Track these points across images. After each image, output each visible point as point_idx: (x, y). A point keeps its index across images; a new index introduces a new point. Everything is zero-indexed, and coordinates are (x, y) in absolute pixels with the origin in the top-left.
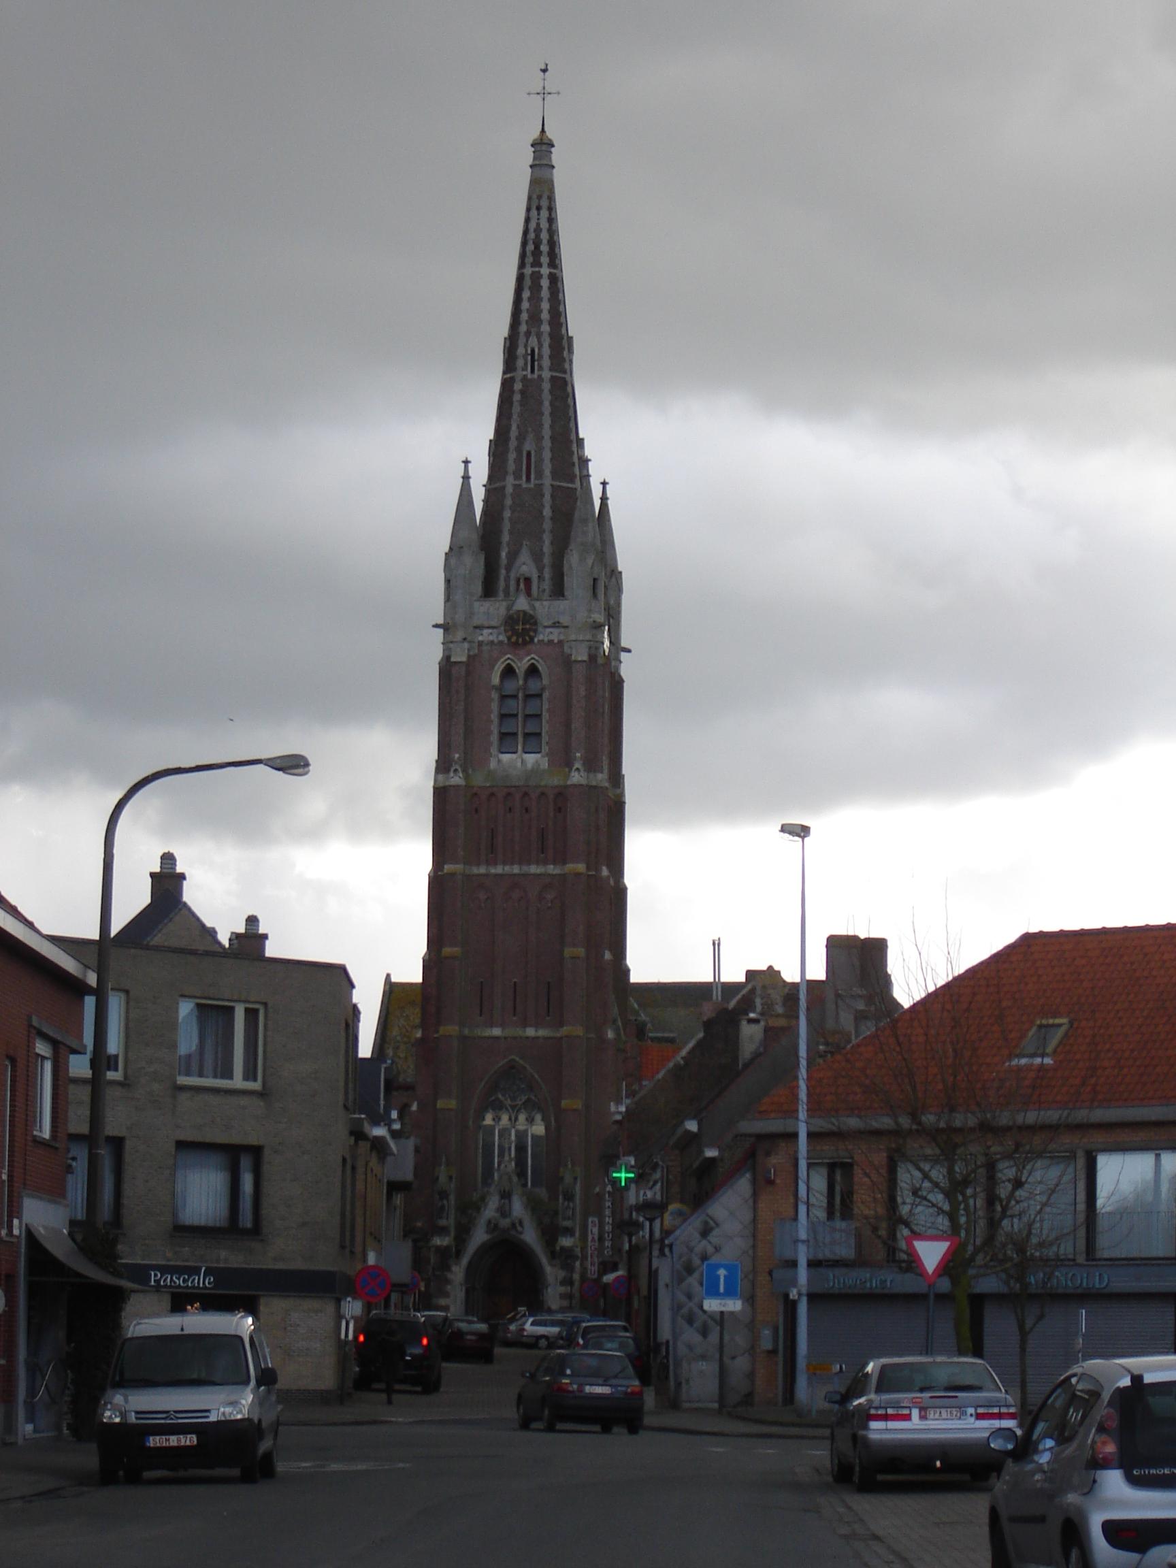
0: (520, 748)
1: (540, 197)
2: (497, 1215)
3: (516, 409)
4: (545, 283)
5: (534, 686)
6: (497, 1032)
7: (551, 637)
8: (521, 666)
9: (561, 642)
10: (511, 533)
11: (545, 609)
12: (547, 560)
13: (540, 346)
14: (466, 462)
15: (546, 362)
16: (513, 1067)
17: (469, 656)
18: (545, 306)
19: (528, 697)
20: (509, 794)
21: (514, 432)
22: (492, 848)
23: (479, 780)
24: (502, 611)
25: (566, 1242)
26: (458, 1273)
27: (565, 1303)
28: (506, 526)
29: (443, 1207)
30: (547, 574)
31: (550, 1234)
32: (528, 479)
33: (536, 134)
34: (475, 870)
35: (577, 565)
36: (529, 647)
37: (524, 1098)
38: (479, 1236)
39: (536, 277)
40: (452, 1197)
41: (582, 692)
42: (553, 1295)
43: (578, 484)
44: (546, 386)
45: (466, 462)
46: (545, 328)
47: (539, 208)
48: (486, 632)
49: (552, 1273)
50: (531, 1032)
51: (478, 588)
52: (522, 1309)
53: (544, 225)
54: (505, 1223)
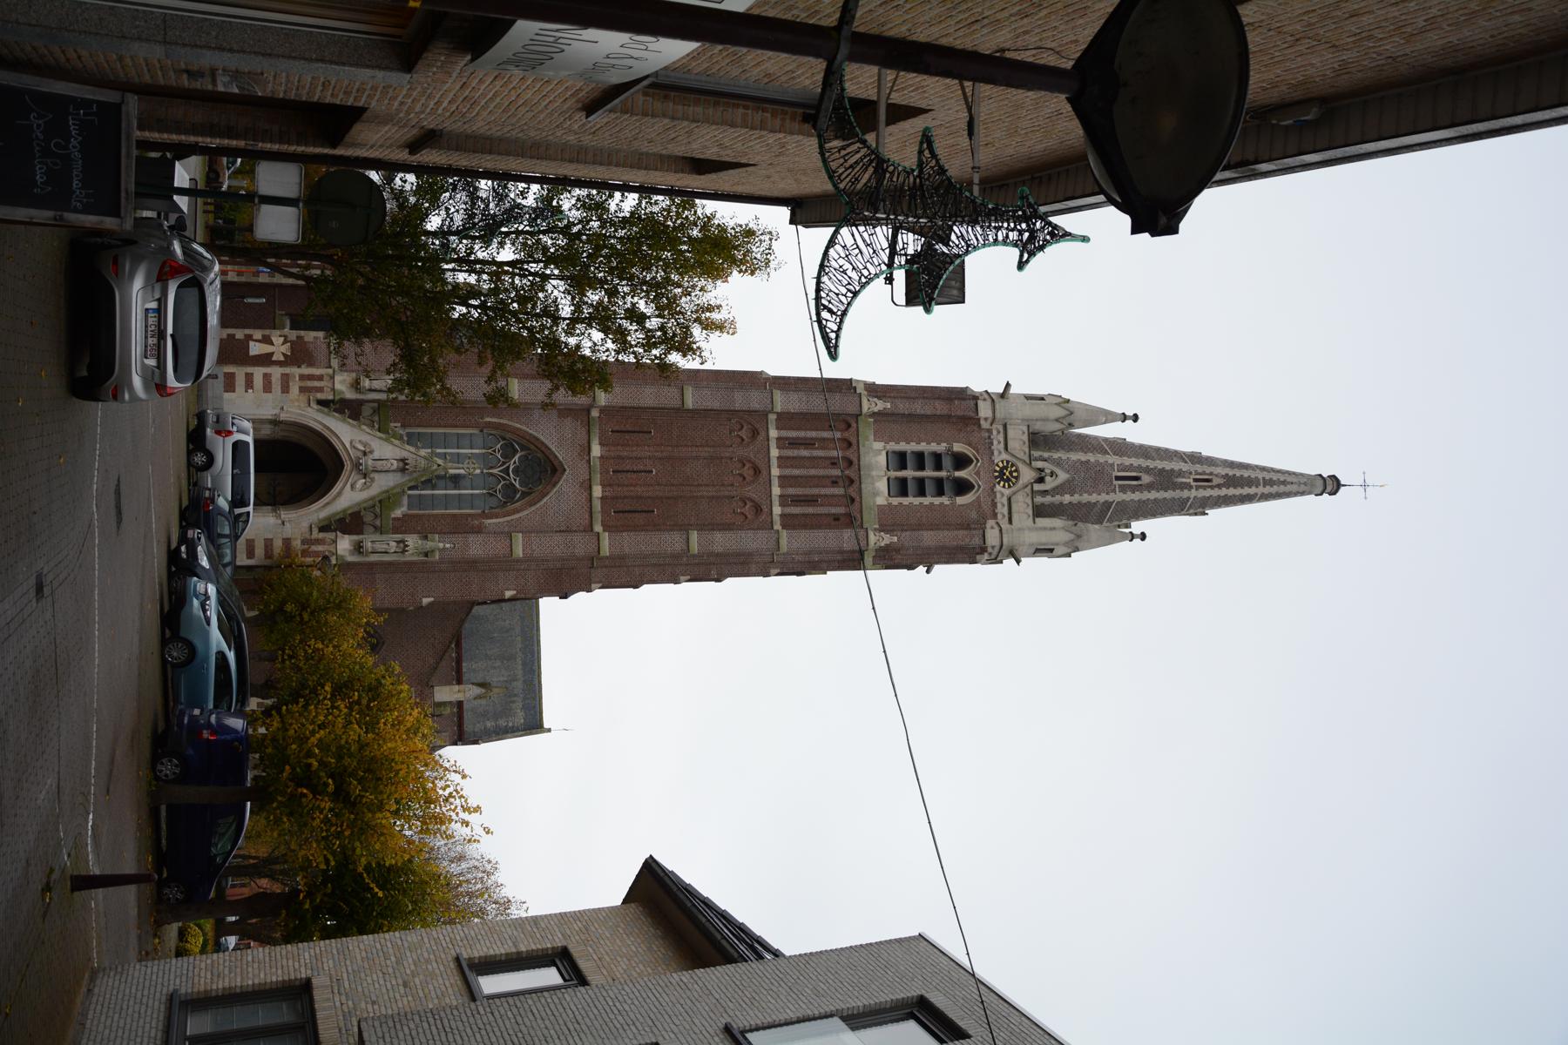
16: (554, 470)
28: (1082, 457)
30: (1048, 499)
32: (1118, 478)
45: (1135, 418)
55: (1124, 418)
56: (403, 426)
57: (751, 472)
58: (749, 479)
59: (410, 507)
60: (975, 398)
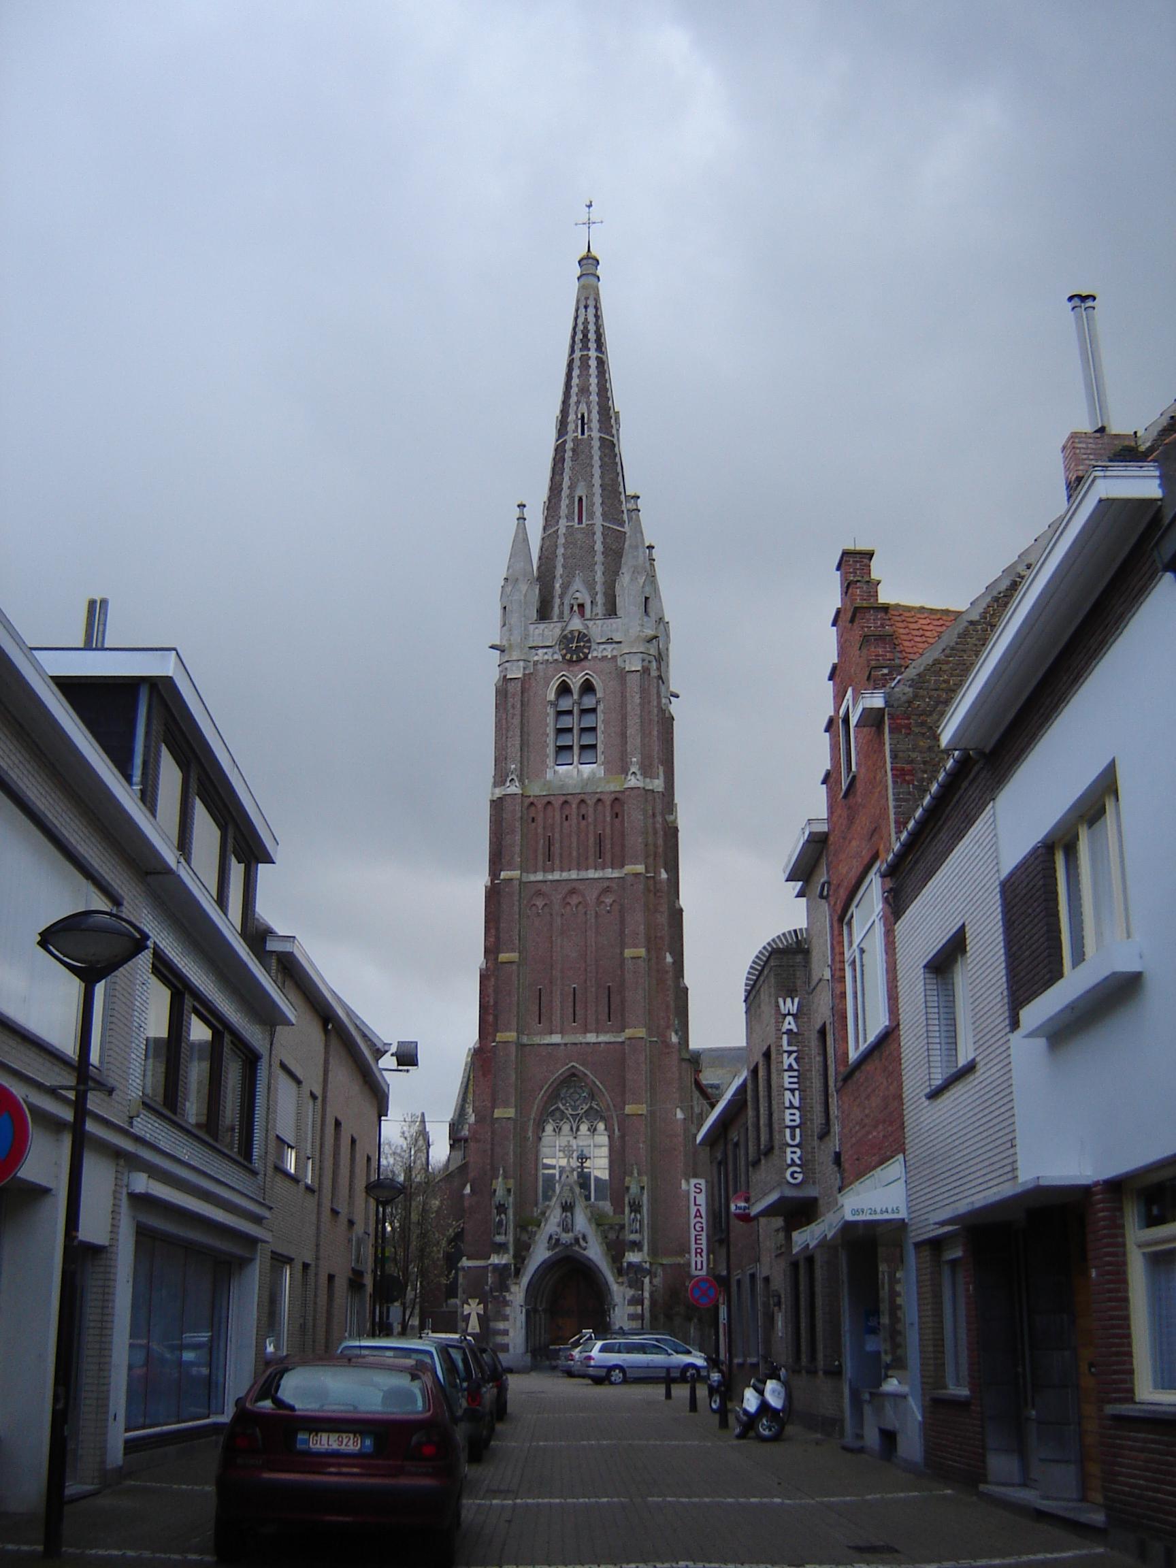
0: (576, 758)
1: (587, 299)
2: (559, 1230)
3: (568, 464)
4: (593, 363)
5: (588, 702)
6: (556, 1039)
7: (605, 653)
8: (575, 683)
9: (614, 657)
10: (563, 566)
11: (598, 629)
12: (599, 588)
13: (590, 412)
14: (522, 506)
15: (595, 425)
16: (574, 1075)
17: (524, 675)
18: (594, 381)
19: (584, 712)
20: (566, 802)
21: (566, 483)
22: (549, 857)
23: (535, 790)
24: (558, 631)
25: (633, 1257)
26: (517, 1294)
27: (635, 1325)
28: (560, 561)
29: (501, 1221)
30: (600, 599)
31: (616, 1249)
32: (580, 521)
33: (584, 252)
34: (532, 878)
35: (628, 589)
36: (583, 663)
37: (586, 1107)
38: (540, 1254)
39: (585, 360)
40: (511, 1212)
41: (637, 700)
42: (621, 1315)
43: (627, 529)
44: (596, 444)
46: (594, 398)
47: (586, 307)
48: (541, 651)
49: (619, 1291)
50: (591, 1038)
51: (534, 615)
52: (587, 1332)
53: (591, 319)
54: (566, 1238)
55: (522, 519)
56: (536, 1205)
57: (574, 896)
58: (581, 899)
59: (604, 1199)
60: (505, 680)
